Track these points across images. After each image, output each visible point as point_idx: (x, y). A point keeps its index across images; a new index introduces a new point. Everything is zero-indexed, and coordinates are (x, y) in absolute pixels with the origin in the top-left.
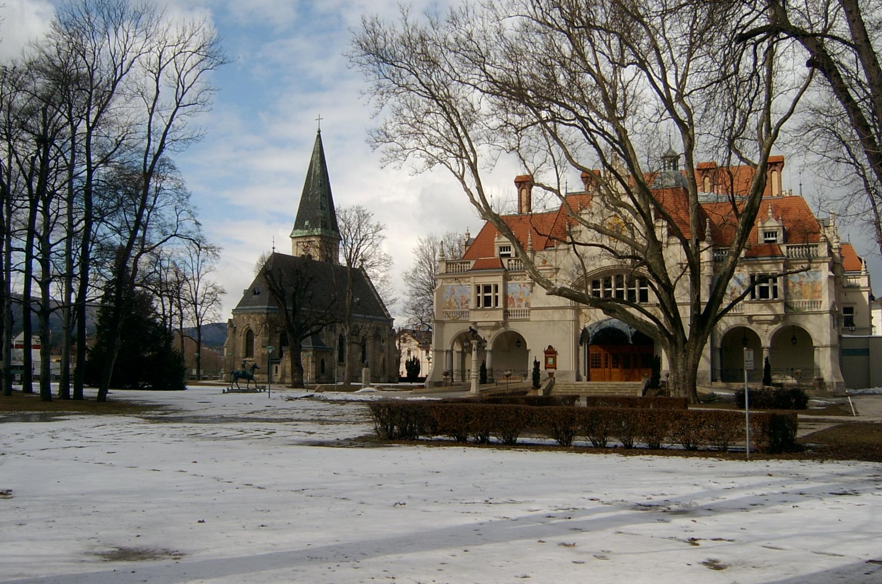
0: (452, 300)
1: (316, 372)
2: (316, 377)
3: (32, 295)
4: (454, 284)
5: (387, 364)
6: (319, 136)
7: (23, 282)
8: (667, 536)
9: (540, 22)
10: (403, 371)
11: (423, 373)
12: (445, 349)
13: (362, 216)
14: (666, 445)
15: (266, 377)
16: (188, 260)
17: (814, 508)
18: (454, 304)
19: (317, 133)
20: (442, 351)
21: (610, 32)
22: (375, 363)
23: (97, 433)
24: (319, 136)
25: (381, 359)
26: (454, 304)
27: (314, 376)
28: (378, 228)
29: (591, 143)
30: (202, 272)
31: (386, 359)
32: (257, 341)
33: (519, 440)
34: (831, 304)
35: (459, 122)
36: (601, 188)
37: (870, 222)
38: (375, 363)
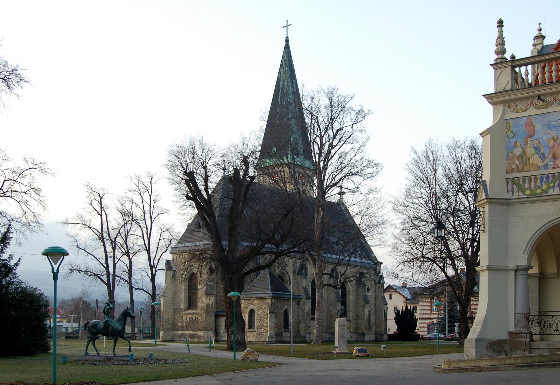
0: (530, 150)
1: (277, 326)
2: (277, 334)
3: (57, 352)
4: (532, 111)
5: (373, 318)
6: (287, 47)
7: (267, 118)
8: (82, 267)
9: (331, 118)
10: (392, 327)
11: (421, 328)
12: (512, 264)
13: (337, 107)
14: (177, 340)
15: (212, 334)
16: (138, 200)
17: (556, 370)
18: (535, 160)
19: (284, 43)
20: (506, 270)
21: (293, 218)
22: (358, 317)
23: (9, 362)
24: (287, 47)
25: (366, 312)
26: (535, 160)
27: (273, 333)
28: (361, 114)
29: (147, 250)
30: (154, 216)
31: (373, 312)
32: (201, 289)
33: (247, 269)
34: (165, 357)
35: (300, 201)
36: (206, 197)
37: (67, 219)
38: (358, 317)
